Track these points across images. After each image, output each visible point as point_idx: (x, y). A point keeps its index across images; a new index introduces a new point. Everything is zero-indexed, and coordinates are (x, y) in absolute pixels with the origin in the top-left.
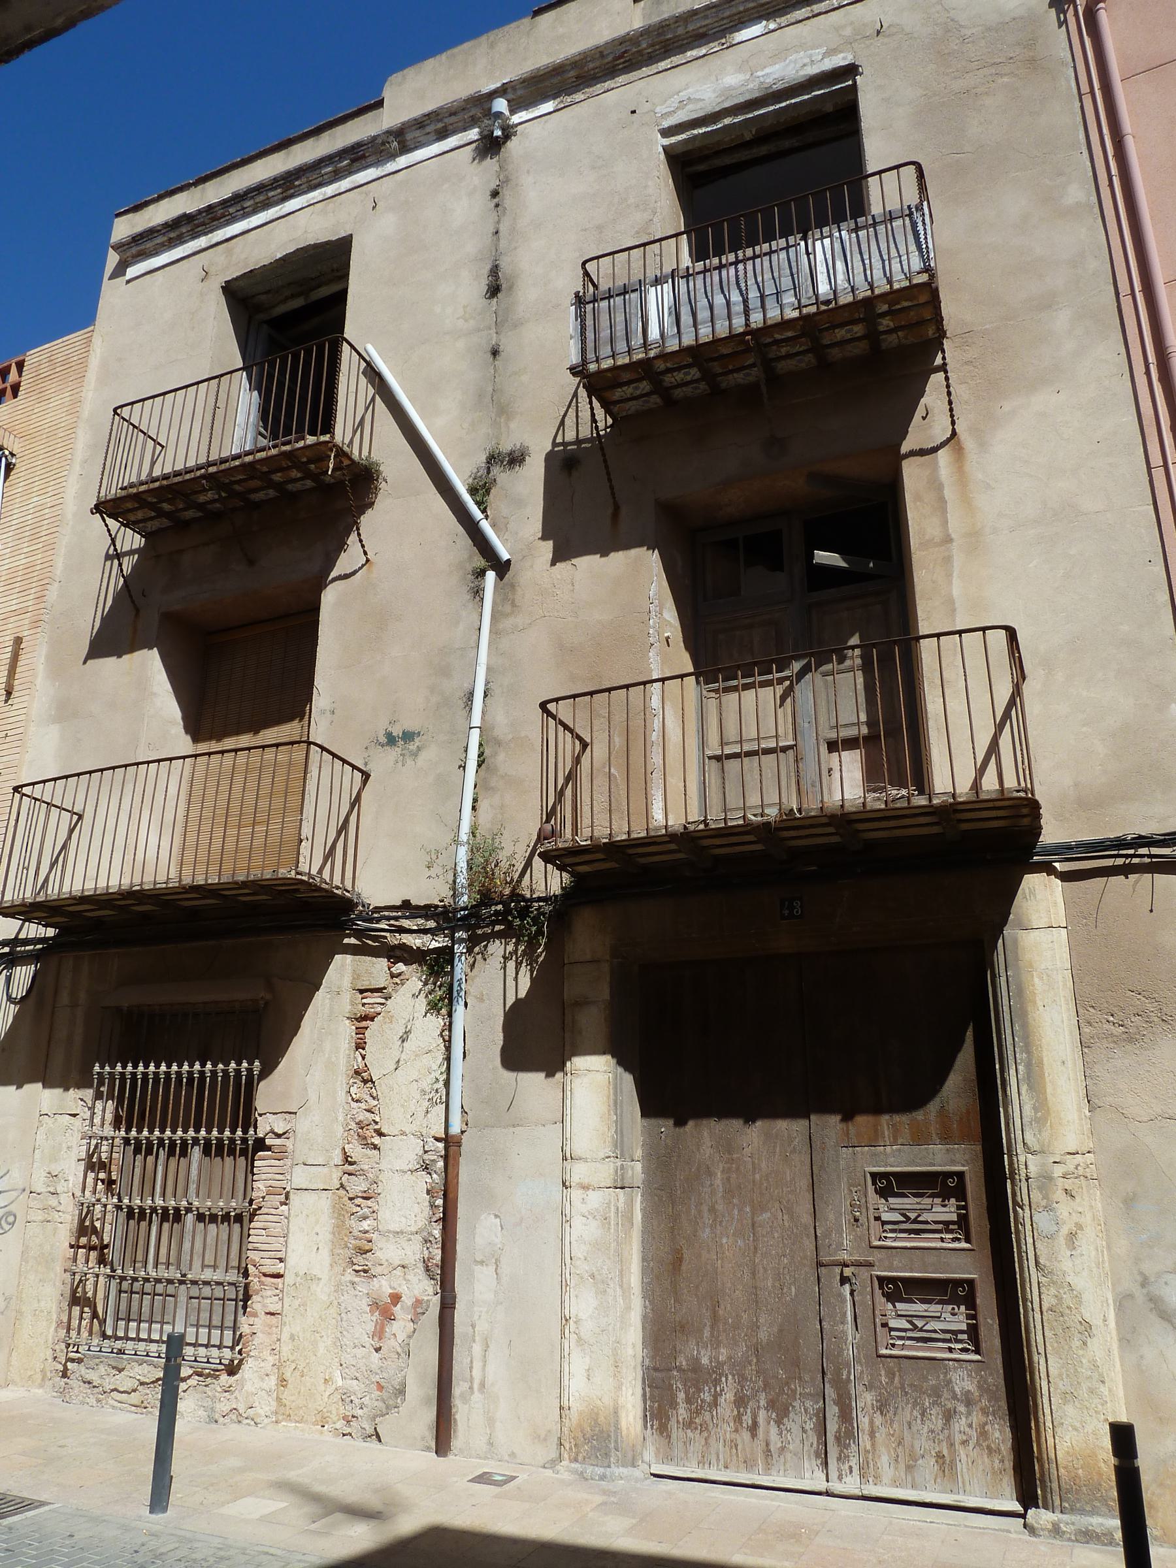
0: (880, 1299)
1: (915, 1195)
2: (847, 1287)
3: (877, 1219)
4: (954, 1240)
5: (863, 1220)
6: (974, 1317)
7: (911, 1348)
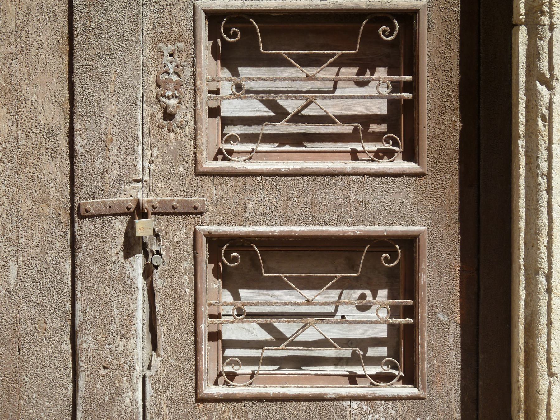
0: (210, 282)
1: (305, 61)
2: (139, 260)
3: (214, 112)
4: (379, 155)
5: (183, 114)
6: (410, 311)
7: (269, 379)
